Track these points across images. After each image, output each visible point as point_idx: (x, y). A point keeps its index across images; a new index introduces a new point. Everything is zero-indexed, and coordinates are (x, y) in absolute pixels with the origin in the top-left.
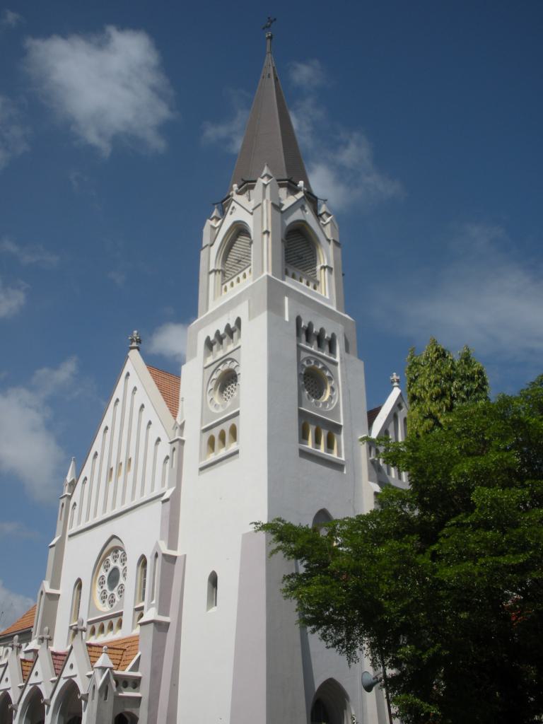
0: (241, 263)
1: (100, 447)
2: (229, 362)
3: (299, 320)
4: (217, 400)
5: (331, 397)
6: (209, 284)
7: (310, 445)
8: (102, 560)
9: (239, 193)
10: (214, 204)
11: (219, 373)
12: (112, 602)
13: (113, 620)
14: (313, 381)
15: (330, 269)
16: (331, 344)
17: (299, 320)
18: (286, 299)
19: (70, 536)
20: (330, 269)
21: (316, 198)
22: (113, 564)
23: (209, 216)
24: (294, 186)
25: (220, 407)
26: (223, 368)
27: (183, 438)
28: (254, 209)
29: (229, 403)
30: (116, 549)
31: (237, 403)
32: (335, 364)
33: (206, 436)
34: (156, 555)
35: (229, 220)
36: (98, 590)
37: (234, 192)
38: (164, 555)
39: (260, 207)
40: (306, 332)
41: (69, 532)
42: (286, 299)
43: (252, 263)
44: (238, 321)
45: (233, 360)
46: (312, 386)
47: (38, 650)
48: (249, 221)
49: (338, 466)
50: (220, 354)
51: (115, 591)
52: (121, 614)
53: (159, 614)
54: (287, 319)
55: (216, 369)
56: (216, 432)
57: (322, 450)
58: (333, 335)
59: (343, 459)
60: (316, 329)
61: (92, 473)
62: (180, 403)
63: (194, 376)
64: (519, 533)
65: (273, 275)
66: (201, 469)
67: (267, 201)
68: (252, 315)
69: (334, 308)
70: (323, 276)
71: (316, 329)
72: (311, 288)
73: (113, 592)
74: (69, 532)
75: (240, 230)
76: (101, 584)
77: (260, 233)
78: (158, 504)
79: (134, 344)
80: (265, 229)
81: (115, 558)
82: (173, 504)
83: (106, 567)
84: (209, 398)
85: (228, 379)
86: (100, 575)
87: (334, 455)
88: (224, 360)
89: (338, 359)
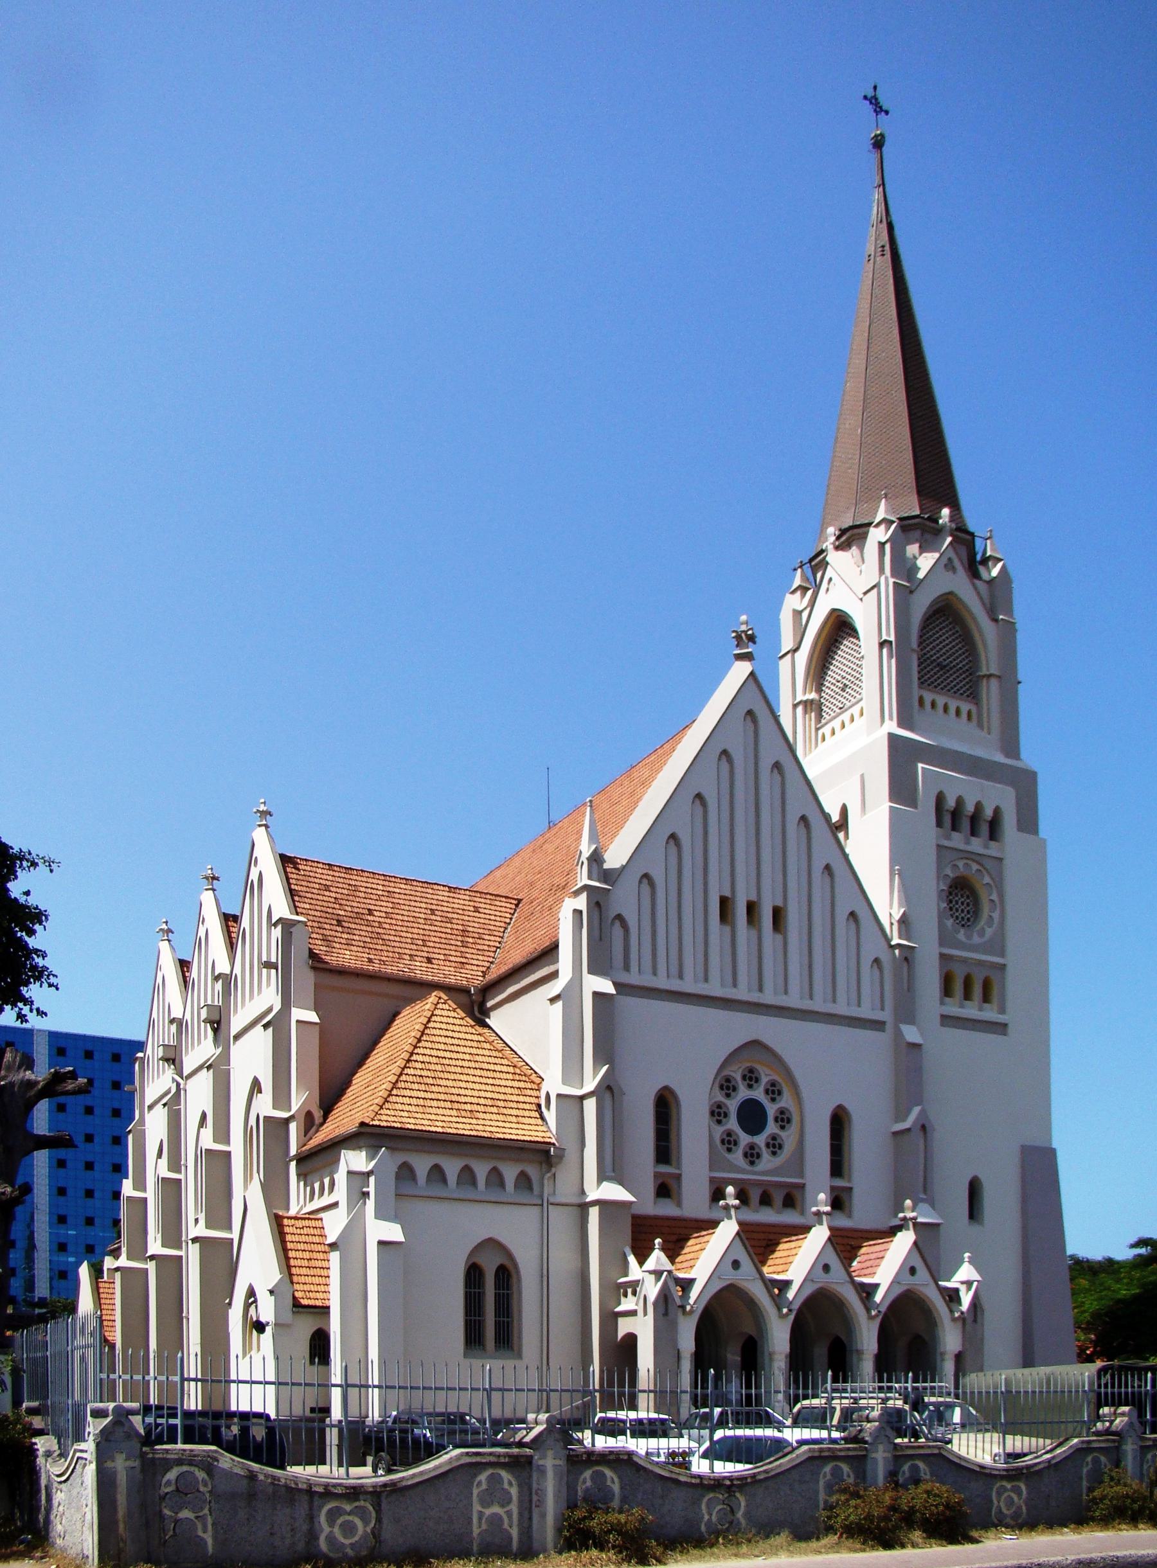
0: (764, 1243)
2: (975, 867)
9: (837, 548)
10: (795, 570)
16: (994, 828)
21: (972, 535)
23: (787, 588)
24: (933, 525)
28: (865, 593)
37: (831, 547)
39: (875, 590)
40: (952, 816)
43: (864, 695)
46: (968, 905)
53: (564, 1083)
58: (997, 811)
64: (619, 1521)
65: (901, 724)
67: (886, 578)
74: (148, 1102)
75: (840, 628)
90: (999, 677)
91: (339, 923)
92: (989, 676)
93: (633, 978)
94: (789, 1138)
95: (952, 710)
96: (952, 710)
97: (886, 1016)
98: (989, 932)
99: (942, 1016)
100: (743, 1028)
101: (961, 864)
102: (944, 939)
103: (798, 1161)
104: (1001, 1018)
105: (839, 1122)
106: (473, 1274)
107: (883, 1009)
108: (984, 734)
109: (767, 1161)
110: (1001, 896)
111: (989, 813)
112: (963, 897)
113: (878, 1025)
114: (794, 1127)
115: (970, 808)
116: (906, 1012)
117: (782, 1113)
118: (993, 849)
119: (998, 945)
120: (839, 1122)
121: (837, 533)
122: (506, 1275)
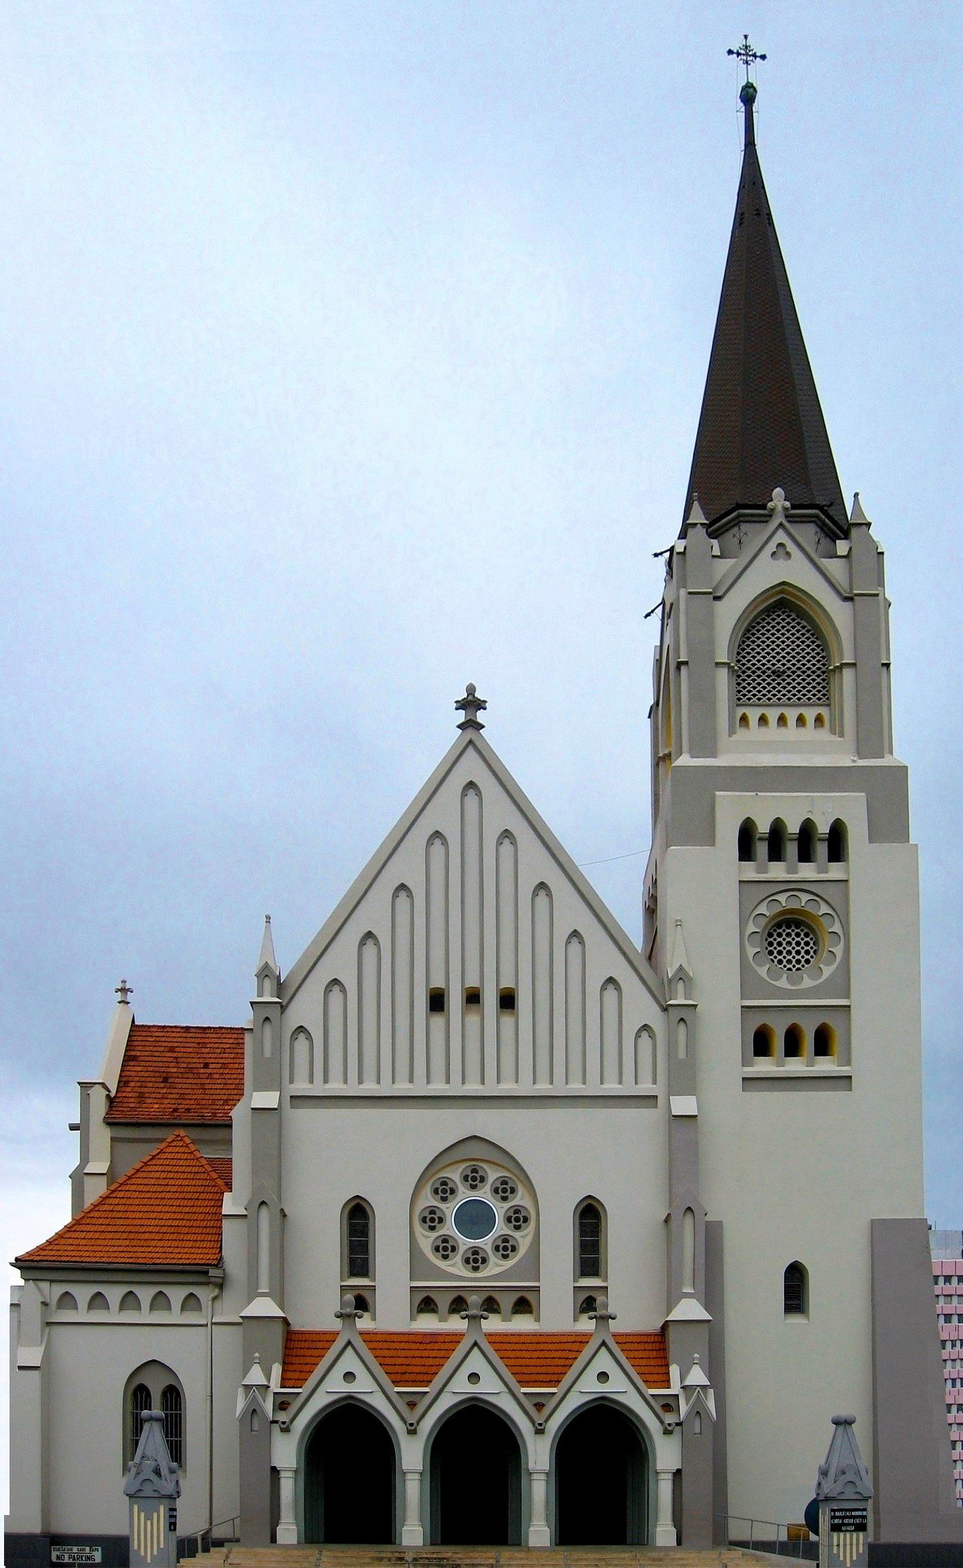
2: (805, 897)
12: (475, 1260)
90: (854, 665)
91: (165, 1080)
92: (843, 665)
93: (301, 1087)
94: (523, 1239)
95: (792, 721)
96: (792, 721)
97: (657, 1090)
98: (828, 971)
99: (744, 1079)
100: (451, 1126)
101: (782, 898)
102: (748, 983)
103: (533, 1262)
104: (844, 1070)
105: (590, 1216)
106: (138, 1395)
107: (411, 1081)
108: (835, 738)
109: (496, 1266)
110: (846, 926)
111: (823, 828)
112: (792, 932)
113: (649, 1100)
114: (530, 1228)
115: (793, 828)
116: (684, 1076)
117: (517, 1212)
118: (835, 871)
119: (843, 983)
120: (590, 1216)
121: (808, 533)
122: (173, 1395)
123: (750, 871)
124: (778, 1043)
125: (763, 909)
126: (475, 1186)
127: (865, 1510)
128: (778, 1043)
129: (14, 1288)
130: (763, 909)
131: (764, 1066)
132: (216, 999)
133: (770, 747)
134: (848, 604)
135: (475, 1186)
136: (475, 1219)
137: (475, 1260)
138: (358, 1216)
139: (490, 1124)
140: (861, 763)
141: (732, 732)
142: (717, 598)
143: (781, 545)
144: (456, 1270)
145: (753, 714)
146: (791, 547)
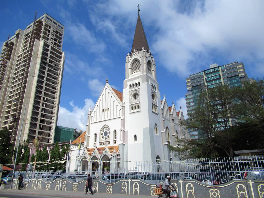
1: (99, 104)
2: (136, 91)
3: (151, 83)
4: (133, 98)
5: (156, 100)
6: (128, 72)
7: (153, 110)
8: (102, 129)
9: (136, 51)
11: (133, 93)
12: (106, 139)
13: (102, 143)
14: (153, 96)
15: (154, 71)
16: (155, 88)
17: (151, 83)
18: (149, 79)
19: (91, 123)
20: (154, 71)
22: (105, 131)
25: (18, 69)
26: (136, 92)
27: (125, 106)
29: (137, 100)
30: (106, 128)
31: (139, 100)
32: (156, 93)
33: (131, 106)
34: (121, 130)
35: (133, 58)
36: (101, 136)
38: (123, 131)
41: (91, 123)
42: (149, 79)
44: (139, 83)
45: (137, 91)
47: (170, 142)
48: (140, 59)
49: (157, 114)
50: (134, 89)
51: (107, 136)
52: (110, 141)
54: (149, 83)
55: (133, 92)
56: (134, 106)
57: (155, 111)
59: (158, 113)
60: (153, 86)
61: (97, 109)
62: (123, 98)
63: (126, 92)
66: (130, 113)
68: (143, 82)
69: (155, 80)
70: (153, 73)
71: (153, 86)
72: (151, 75)
73: (106, 136)
74: (91, 123)
76: (102, 134)
77: (143, 63)
78: (120, 119)
79: (107, 82)
80: (144, 63)
81: (106, 129)
82: (123, 120)
83: (103, 131)
84: (131, 98)
85: (136, 95)
86: (101, 133)
87: (156, 112)
88: (135, 90)
89: (156, 92)
100: (102, 124)
116: (124, 114)
123: (131, 90)
124: (137, 107)
125: (132, 93)
126: (105, 131)
127: (55, 89)
128: (137, 107)
129: (70, 109)
130: (132, 93)
131: (133, 111)
132: (34, 78)
133: (136, 75)
134: (141, 58)
135: (105, 131)
136: (106, 134)
137: (106, 139)
138: (96, 134)
139: (106, 123)
140: (143, 74)
141: (130, 75)
142: (129, 62)
143: (135, 55)
144: (104, 140)
145: (133, 72)
146: (136, 54)
